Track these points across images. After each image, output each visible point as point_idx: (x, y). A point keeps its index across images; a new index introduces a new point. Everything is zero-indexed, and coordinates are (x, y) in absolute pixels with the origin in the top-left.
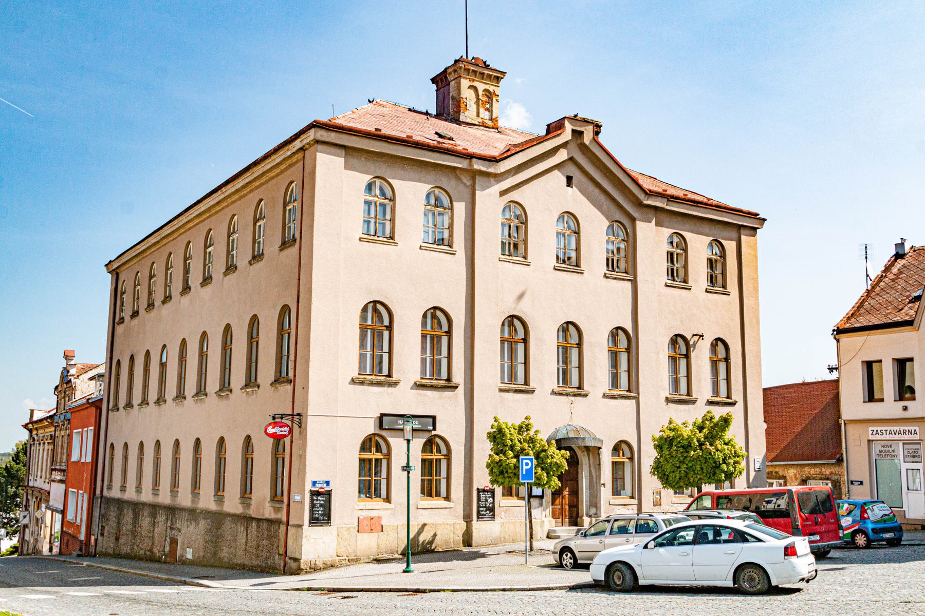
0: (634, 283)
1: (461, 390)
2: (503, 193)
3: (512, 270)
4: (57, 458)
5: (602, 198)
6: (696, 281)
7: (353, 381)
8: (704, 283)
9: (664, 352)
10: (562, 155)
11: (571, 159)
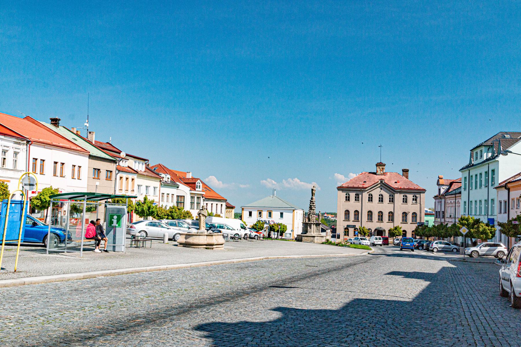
0: (394, 204)
2: (367, 193)
3: (370, 204)
4: (471, 211)
5: (388, 191)
7: (343, 221)
9: (474, 202)
10: (379, 185)
11: (381, 186)
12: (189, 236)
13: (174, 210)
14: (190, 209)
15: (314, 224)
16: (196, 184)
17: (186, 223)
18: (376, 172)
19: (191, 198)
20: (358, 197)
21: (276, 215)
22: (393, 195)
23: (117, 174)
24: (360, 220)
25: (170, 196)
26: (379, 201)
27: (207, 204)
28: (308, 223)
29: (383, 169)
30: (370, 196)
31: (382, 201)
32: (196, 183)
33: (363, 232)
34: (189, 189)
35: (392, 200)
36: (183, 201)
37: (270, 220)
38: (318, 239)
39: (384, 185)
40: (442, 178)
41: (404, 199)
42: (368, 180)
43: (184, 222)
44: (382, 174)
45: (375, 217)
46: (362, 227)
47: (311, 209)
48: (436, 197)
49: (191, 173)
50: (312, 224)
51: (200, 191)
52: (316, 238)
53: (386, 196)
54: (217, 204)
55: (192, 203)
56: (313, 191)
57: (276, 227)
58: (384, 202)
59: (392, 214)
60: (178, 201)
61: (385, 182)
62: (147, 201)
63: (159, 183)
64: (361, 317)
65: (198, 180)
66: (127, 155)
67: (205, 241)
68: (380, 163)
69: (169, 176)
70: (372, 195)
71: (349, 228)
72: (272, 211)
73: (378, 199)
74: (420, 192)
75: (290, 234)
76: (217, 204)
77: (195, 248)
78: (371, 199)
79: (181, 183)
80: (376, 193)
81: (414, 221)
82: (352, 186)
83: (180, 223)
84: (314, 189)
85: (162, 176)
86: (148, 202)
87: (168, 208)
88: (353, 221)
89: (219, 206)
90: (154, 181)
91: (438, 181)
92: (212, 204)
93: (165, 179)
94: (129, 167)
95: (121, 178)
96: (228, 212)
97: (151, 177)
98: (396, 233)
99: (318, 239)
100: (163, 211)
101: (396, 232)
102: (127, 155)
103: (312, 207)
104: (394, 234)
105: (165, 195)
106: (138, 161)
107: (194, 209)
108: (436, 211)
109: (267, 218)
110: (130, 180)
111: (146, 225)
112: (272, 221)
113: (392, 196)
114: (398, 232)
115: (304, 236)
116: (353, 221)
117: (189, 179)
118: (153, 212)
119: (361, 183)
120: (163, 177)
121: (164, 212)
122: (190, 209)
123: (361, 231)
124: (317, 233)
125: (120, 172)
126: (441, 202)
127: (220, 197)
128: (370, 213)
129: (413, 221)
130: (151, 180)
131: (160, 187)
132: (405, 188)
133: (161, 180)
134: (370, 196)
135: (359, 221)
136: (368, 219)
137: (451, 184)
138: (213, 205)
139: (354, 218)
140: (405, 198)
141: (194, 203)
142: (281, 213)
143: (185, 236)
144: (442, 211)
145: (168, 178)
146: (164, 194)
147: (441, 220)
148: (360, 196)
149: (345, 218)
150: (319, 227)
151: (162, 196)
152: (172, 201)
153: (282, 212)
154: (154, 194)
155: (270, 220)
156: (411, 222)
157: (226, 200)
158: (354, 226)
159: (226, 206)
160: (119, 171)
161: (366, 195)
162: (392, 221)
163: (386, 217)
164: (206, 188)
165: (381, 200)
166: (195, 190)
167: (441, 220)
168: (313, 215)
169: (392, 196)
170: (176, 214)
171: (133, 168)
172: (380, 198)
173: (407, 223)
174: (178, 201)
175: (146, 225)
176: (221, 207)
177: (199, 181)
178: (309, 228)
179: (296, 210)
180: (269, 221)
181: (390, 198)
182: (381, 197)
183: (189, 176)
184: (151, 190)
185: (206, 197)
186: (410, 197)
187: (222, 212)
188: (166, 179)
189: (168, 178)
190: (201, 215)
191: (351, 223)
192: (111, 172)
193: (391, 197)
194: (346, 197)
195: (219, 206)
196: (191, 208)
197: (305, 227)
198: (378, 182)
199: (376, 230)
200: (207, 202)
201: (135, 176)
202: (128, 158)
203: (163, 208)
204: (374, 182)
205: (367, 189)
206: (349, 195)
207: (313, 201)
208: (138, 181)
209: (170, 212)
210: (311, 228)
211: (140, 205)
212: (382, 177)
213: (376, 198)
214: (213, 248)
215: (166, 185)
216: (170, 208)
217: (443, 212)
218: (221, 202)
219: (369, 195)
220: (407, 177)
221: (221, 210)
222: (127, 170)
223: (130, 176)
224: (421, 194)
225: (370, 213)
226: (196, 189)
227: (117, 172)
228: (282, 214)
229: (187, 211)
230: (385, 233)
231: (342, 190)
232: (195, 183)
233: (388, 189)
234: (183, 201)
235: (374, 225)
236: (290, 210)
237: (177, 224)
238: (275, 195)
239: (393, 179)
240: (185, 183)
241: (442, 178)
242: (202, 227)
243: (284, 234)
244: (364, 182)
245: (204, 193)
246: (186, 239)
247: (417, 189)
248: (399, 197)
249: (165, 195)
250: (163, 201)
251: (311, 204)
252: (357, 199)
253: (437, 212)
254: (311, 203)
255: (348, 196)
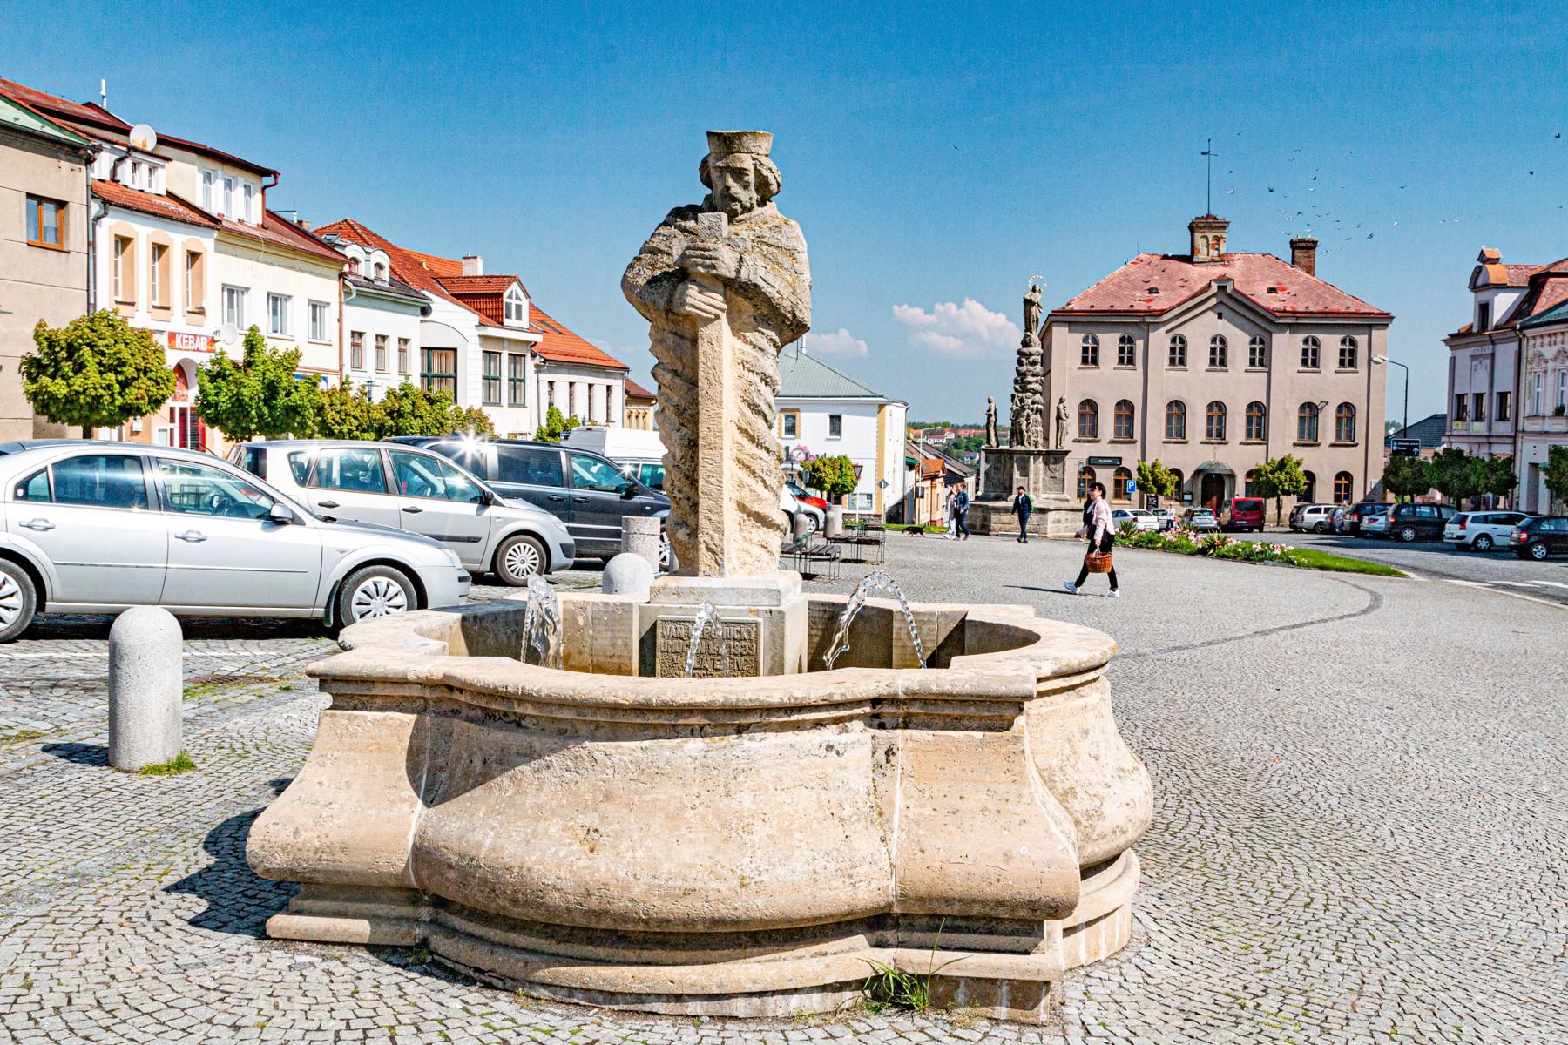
0: (1269, 373)
1: (1139, 444)
2: (1167, 332)
3: (1177, 374)
5: (1245, 323)
6: (1326, 367)
8: (1335, 365)
10: (1214, 301)
12: (496, 736)
13: (407, 406)
14: (484, 404)
15: (1040, 453)
16: (506, 300)
17: (460, 461)
18: (1189, 254)
19: (484, 357)
20: (1131, 351)
21: (813, 424)
22: (1266, 340)
23: (97, 219)
24: (1137, 436)
25: (392, 346)
26: (1213, 362)
27: (551, 384)
28: (1010, 453)
29: (1218, 239)
30: (1178, 345)
31: (1223, 363)
32: (506, 294)
33: (1155, 482)
34: (475, 318)
35: (1261, 358)
36: (450, 372)
37: (792, 443)
38: (1059, 521)
39: (1232, 302)
40: (1495, 261)
41: (1305, 352)
42: (1166, 282)
43: (448, 454)
44: (1213, 261)
45: (1197, 423)
46: (1148, 463)
47: (1024, 390)
48: (1456, 340)
49: (480, 262)
50: (1030, 453)
51: (521, 330)
52: (1051, 516)
53: (1239, 342)
54: (590, 386)
55: (490, 380)
56: (1034, 309)
57: (828, 470)
58: (1229, 367)
59: (1260, 410)
60: (429, 369)
61: (1234, 289)
62: (258, 357)
63: (334, 285)
64: (1232, 854)
65: (510, 285)
66: (161, 141)
67: (866, 844)
68: (1208, 216)
69: (380, 257)
70: (1182, 341)
71: (1096, 470)
72: (798, 410)
73: (1208, 355)
74: (1371, 326)
75: (870, 496)
76: (590, 386)
77: (634, 1003)
78: (1178, 356)
79: (439, 294)
80: (1201, 331)
81: (1254, 433)
82: (1107, 307)
83: (415, 464)
84: (1037, 297)
85: (349, 256)
86: (264, 362)
87: (378, 396)
88: (1112, 442)
89: (600, 392)
90: (311, 273)
91: (1478, 270)
92: (571, 384)
93: (365, 270)
94: (170, 195)
95: (123, 242)
96: (633, 416)
97: (294, 250)
98: (1281, 483)
99: (1059, 521)
100: (349, 408)
101: (1282, 478)
102: (161, 141)
103: (1030, 378)
104: (1275, 487)
105: (369, 343)
106: (221, 172)
107: (498, 404)
108: (1458, 391)
109: (780, 437)
110: (177, 257)
111: (24, 490)
112: (799, 448)
113: (1262, 342)
114: (1291, 480)
115: (997, 510)
116: (1112, 442)
117: (472, 280)
118: (293, 410)
119: (1138, 294)
120: (355, 261)
121: (357, 413)
122: (484, 404)
123: (1145, 479)
124: (1053, 496)
125: (112, 210)
126: (1493, 355)
127: (594, 354)
128: (1177, 410)
129: (1338, 436)
130: (293, 268)
131: (340, 304)
132: (1311, 309)
133: (346, 268)
134: (1178, 345)
135: (1135, 442)
136: (1169, 433)
137: (1537, 283)
138: (576, 388)
139: (1116, 428)
140: (1310, 347)
141: (498, 379)
142: (831, 417)
143: (405, 721)
144: (1498, 388)
145: (379, 266)
146: (360, 334)
147: (1490, 429)
148: (1139, 345)
149: (1080, 430)
150: (1058, 467)
151: (353, 345)
152: (402, 369)
153: (835, 413)
154: (314, 336)
155: (792, 443)
156: (1333, 441)
157: (627, 369)
158: (1115, 462)
159: (627, 392)
160: (106, 203)
161: (1160, 341)
162: (1258, 436)
163: (1236, 424)
164: (542, 321)
165: (1219, 357)
166: (502, 324)
167: (1490, 429)
168: (1033, 417)
169: (1262, 342)
170: (416, 423)
171: (199, 204)
172: (1213, 351)
173: (1319, 445)
174: (429, 369)
175: (24, 490)
176: (608, 396)
177: (514, 287)
178: (1017, 474)
179: (889, 402)
180: (787, 449)
181: (1253, 351)
182: (1218, 346)
183: (477, 268)
184: (297, 314)
185: (548, 357)
186: (1331, 344)
187: (612, 418)
188: (368, 268)
189: (379, 266)
190: (697, 299)
191: (1104, 449)
192: (61, 205)
193: (1257, 347)
194: (1085, 350)
195: (600, 392)
196: (488, 401)
197: (997, 469)
198: (1209, 286)
199: (1198, 472)
200: (551, 377)
201: (205, 242)
202: (165, 151)
203: (352, 393)
204: (1190, 289)
205: (1165, 318)
206: (1095, 341)
207: (1031, 355)
208: (222, 266)
209: (390, 414)
210: (1025, 473)
211: (224, 378)
212: (1218, 271)
213: (1199, 353)
214: (1026, 993)
215: (368, 294)
216: (391, 393)
217: (1503, 396)
218: (608, 375)
219: (1173, 340)
220: (1310, 270)
221: (608, 408)
222: (160, 206)
223: (179, 240)
224: (1374, 332)
225: (1177, 410)
226: (506, 322)
227: (96, 207)
228: (835, 420)
229: (469, 411)
230: (1234, 483)
231: (1069, 323)
232: (500, 295)
233: (1247, 314)
234: (450, 372)
235: (1192, 456)
236: (871, 404)
237: (389, 475)
238: (804, 351)
239: (1258, 277)
240: (459, 297)
241: (1495, 261)
242: (731, 516)
243: (846, 498)
244: (1151, 291)
245: (538, 338)
246: (433, 794)
247: (1357, 314)
248: (1287, 347)
249: (369, 343)
250: (357, 366)
251: (1024, 369)
252: (1126, 357)
253: (1461, 397)
254: (1020, 363)
255: (1090, 345)
